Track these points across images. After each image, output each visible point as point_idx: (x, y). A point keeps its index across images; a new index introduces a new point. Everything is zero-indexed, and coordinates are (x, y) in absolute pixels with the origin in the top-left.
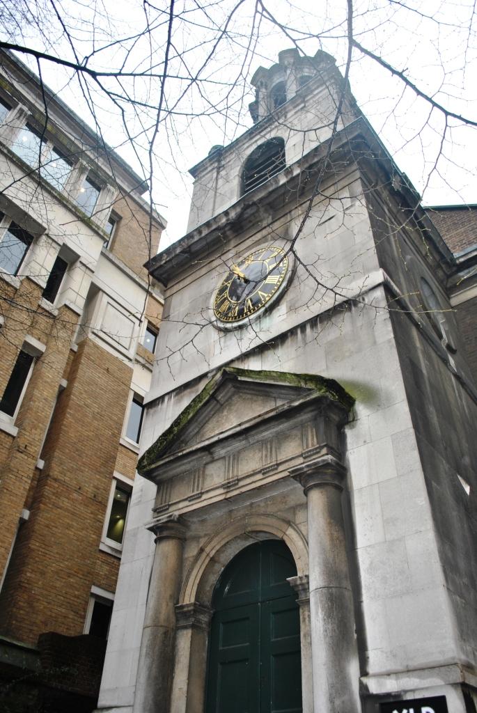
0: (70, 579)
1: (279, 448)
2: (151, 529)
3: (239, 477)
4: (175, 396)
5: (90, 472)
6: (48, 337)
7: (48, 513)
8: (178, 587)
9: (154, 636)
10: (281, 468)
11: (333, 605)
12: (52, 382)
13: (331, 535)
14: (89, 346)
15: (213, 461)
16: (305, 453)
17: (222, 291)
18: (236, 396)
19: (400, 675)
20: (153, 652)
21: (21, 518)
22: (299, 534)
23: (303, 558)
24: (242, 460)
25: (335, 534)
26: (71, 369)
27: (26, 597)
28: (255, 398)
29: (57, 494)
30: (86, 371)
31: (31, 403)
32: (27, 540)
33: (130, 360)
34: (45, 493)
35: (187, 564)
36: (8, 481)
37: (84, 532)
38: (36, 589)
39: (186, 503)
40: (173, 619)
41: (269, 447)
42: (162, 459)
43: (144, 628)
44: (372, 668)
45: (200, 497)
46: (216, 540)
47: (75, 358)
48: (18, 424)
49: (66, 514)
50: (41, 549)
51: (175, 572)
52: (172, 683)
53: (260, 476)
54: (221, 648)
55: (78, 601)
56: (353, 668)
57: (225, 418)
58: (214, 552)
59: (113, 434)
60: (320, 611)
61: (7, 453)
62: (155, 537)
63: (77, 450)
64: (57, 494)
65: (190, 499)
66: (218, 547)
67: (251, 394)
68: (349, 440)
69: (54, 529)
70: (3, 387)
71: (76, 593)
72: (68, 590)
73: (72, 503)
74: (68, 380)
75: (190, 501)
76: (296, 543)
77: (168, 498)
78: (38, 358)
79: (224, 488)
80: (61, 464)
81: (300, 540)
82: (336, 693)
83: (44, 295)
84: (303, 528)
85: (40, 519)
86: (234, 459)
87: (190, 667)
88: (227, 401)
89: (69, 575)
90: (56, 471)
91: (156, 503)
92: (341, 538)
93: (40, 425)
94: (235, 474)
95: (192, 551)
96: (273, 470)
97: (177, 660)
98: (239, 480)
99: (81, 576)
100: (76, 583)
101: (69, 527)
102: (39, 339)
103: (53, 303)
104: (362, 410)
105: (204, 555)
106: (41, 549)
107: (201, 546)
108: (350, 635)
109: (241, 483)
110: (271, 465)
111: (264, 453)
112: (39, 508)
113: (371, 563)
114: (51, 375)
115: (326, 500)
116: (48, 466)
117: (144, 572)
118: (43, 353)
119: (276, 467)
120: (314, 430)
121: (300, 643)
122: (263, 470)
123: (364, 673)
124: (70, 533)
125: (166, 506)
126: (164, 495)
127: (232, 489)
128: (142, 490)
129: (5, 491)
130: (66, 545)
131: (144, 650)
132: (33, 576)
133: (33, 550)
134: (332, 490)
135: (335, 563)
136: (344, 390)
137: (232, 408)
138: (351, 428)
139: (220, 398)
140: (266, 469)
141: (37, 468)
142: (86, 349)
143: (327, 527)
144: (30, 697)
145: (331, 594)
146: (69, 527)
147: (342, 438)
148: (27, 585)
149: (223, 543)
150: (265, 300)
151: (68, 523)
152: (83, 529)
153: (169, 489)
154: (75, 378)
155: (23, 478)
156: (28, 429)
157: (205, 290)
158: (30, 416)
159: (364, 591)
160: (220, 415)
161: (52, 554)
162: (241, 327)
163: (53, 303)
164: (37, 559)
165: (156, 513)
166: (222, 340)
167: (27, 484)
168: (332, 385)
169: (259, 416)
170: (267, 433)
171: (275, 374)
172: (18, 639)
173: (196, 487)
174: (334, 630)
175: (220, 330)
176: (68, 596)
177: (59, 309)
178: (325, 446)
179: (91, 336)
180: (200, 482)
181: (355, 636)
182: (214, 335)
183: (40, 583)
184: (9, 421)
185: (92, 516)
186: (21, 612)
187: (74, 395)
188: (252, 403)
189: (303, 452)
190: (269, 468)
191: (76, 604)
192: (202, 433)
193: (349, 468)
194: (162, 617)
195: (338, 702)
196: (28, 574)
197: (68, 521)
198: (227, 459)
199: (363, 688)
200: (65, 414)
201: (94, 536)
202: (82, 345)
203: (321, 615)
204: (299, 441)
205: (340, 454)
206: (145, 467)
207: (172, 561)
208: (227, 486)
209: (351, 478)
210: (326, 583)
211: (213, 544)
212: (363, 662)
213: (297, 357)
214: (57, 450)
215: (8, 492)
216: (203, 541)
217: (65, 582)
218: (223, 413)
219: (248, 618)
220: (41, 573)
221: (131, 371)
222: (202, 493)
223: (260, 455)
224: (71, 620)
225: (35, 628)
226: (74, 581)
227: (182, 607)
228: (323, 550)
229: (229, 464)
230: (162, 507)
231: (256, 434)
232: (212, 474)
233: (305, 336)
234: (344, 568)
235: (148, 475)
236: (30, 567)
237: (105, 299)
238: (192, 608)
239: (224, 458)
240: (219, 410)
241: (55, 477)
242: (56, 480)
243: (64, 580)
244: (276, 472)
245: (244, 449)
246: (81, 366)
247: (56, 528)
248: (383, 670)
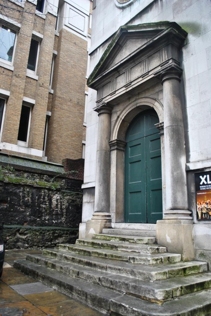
0: (72, 138)
2: (96, 110)
3: (131, 81)
4: (102, 48)
5: (74, 92)
6: (43, 31)
7: (58, 112)
8: (110, 134)
9: (101, 154)
10: (150, 73)
11: (174, 133)
12: (49, 52)
13: (174, 102)
14: (64, 32)
16: (161, 64)
19: (204, 161)
20: (101, 160)
21: (47, 115)
22: (160, 104)
23: (162, 115)
24: (132, 72)
25: (176, 102)
26: (58, 45)
27: (56, 146)
29: (61, 104)
30: (65, 45)
31: (41, 63)
32: (52, 124)
33: (85, 37)
34: (56, 104)
35: (113, 124)
36: (39, 100)
37: (76, 118)
38: (59, 143)
39: (110, 97)
40: (109, 147)
41: (144, 64)
42: (97, 78)
43: (97, 151)
44: (191, 159)
45: (115, 93)
46: (124, 112)
47: (58, 39)
48: (38, 74)
49: (67, 111)
50: (58, 127)
51: (108, 127)
52: (110, 172)
53: (141, 79)
54: (129, 157)
55: (78, 146)
56: (183, 160)
57: (124, 53)
58: (123, 117)
59: (82, 74)
61: (35, 88)
62: (98, 113)
63: (67, 83)
64: (61, 104)
65: (111, 94)
68: (184, 55)
69: (62, 118)
70: (27, 58)
71: (76, 143)
72: (73, 143)
73: (68, 107)
74: (57, 51)
75: (111, 95)
76: (159, 109)
78: (41, 42)
79: (125, 87)
80: (61, 90)
81: (160, 106)
82: (174, 170)
83: (37, 9)
84: (162, 101)
85: (55, 115)
86: (129, 73)
87: (117, 165)
89: (72, 137)
90: (59, 94)
91: (97, 99)
92: (179, 103)
93: (47, 73)
94: (130, 80)
95: (114, 118)
96: (146, 75)
97: (111, 163)
98: (131, 82)
99: (77, 137)
100: (75, 140)
101: (69, 117)
102: (39, 32)
103: (42, 12)
104: (191, 38)
105: (119, 119)
106: (58, 127)
107: (118, 115)
108: (182, 145)
109: (133, 84)
110: (145, 72)
112: (54, 110)
113: (193, 114)
114: (47, 50)
115: (172, 85)
116: (55, 92)
117: (96, 129)
118: (42, 39)
119: (148, 73)
120: (166, 52)
121: (161, 151)
122: (142, 75)
123: (188, 161)
124: (70, 119)
125: (101, 99)
127: (128, 87)
128: (92, 95)
129: (38, 104)
130: (69, 125)
131: (97, 160)
132: (57, 138)
133: (55, 128)
135: (176, 114)
136: (181, 28)
137: (127, 48)
138: (185, 49)
139: (121, 43)
140: (143, 75)
141: (50, 93)
142: (63, 34)
143: (172, 99)
144: (62, 182)
145: (173, 129)
146: (69, 117)
147: (180, 54)
148: (55, 142)
151: (68, 115)
152: (75, 117)
153: (102, 90)
154: (60, 50)
155: (44, 98)
156: (42, 75)
158: (42, 70)
160: (122, 52)
161: (63, 129)
163: (42, 12)
164: (57, 131)
166: (122, 13)
167: (46, 100)
168: (174, 25)
169: (139, 48)
171: (145, 25)
172: (55, 162)
174: (174, 144)
175: (120, 8)
176: (73, 145)
177: (46, 15)
178: (172, 58)
179: (64, 27)
180: (115, 86)
181: (185, 146)
182: (119, 11)
183: (60, 140)
184: (33, 74)
185: (78, 111)
186: (55, 152)
187: (61, 58)
188: (136, 43)
189: (161, 63)
190: (145, 74)
191: (77, 147)
193: (184, 69)
194: (104, 146)
195: (175, 174)
196: (55, 138)
197: (68, 114)
199: (187, 167)
200: (58, 67)
201: (80, 120)
202: (60, 33)
205: (179, 63)
206: (90, 83)
207: (106, 123)
208: (126, 86)
209: (185, 73)
210: (171, 124)
211: (123, 113)
212: (188, 157)
213: (158, 15)
214: (58, 84)
215: (39, 105)
216: (119, 113)
217: (71, 140)
218: (123, 51)
219: (140, 144)
220: (60, 137)
221: (87, 42)
222: (116, 91)
223: (140, 69)
224: (76, 154)
225: (61, 158)
226: (75, 139)
227: (112, 142)
228: (170, 110)
230: (100, 100)
231: (138, 59)
232: (120, 82)
233: (162, 2)
234: (180, 117)
235: (92, 86)
236: (55, 135)
237: (68, 6)
238: (116, 141)
241: (59, 96)
242: (59, 97)
243: (70, 139)
244: (148, 75)
246: (62, 43)
247: (63, 118)
248: (197, 160)
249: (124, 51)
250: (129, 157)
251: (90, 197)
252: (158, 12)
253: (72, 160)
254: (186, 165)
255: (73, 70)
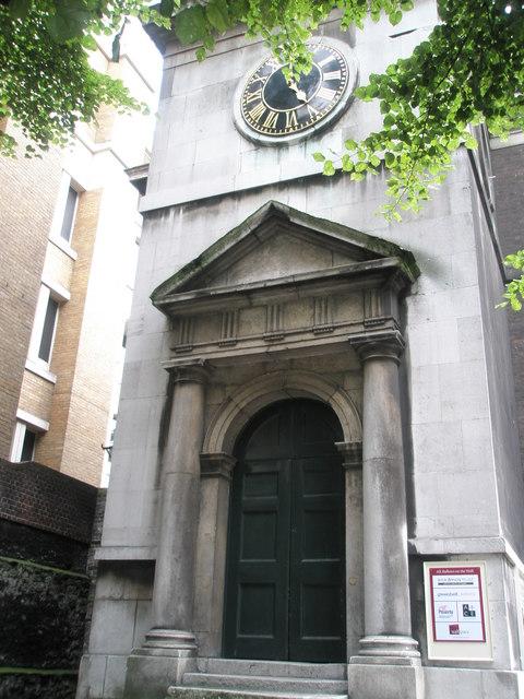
1: (335, 310)
15: (251, 307)
17: (253, 87)
18: (281, 237)
28: (306, 245)
39: (215, 348)
44: (419, 532)
60: (378, 478)
66: (250, 399)
67: (301, 239)
68: (411, 314)
77: (191, 338)
86: (279, 310)
88: (269, 239)
104: (426, 283)
105: (232, 405)
109: (288, 339)
111: (317, 312)
123: (411, 535)
126: (186, 335)
134: (394, 365)
149: (255, 396)
150: (315, 119)
153: (191, 332)
157: (225, 77)
159: (415, 465)
162: (279, 146)
165: (174, 354)
170: (321, 291)
173: (229, 332)
192: (234, 270)
198: (270, 308)
199: (411, 548)
203: (378, 483)
204: (360, 307)
213: (353, 204)
222: (237, 341)
227: (208, 456)
229: (272, 314)
239: (265, 307)
240: (257, 247)
245: (292, 302)
249: (266, 253)
250: (244, 498)
251: (124, 586)
252: (353, 197)
253: (51, 470)
254: (409, 544)
255: (25, 202)
